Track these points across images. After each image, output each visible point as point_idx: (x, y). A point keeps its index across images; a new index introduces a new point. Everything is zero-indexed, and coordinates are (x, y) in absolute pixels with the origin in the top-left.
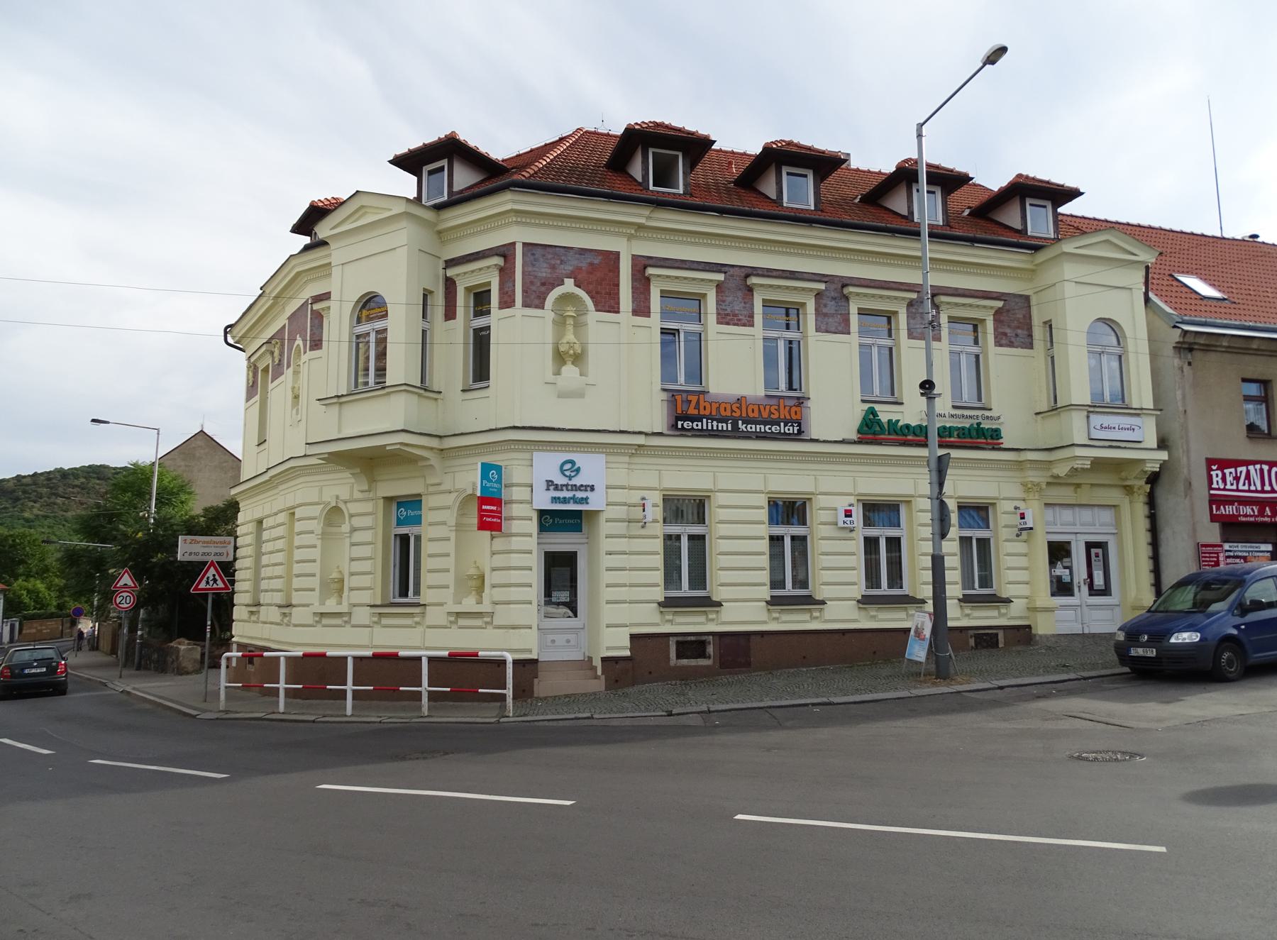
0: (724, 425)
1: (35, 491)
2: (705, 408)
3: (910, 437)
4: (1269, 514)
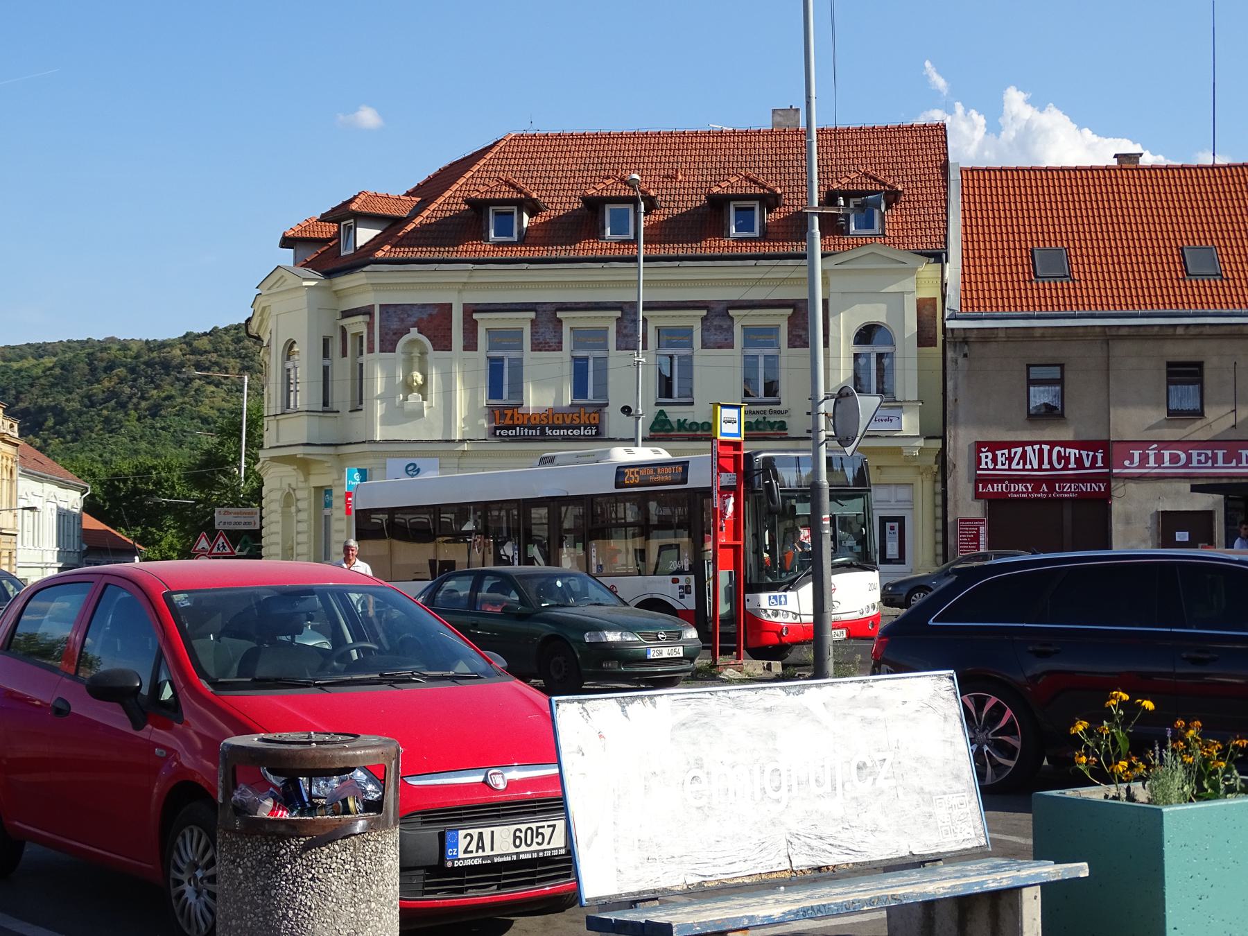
0: (534, 431)
1: (216, 364)
2: (518, 419)
3: (699, 433)
4: (1046, 490)
